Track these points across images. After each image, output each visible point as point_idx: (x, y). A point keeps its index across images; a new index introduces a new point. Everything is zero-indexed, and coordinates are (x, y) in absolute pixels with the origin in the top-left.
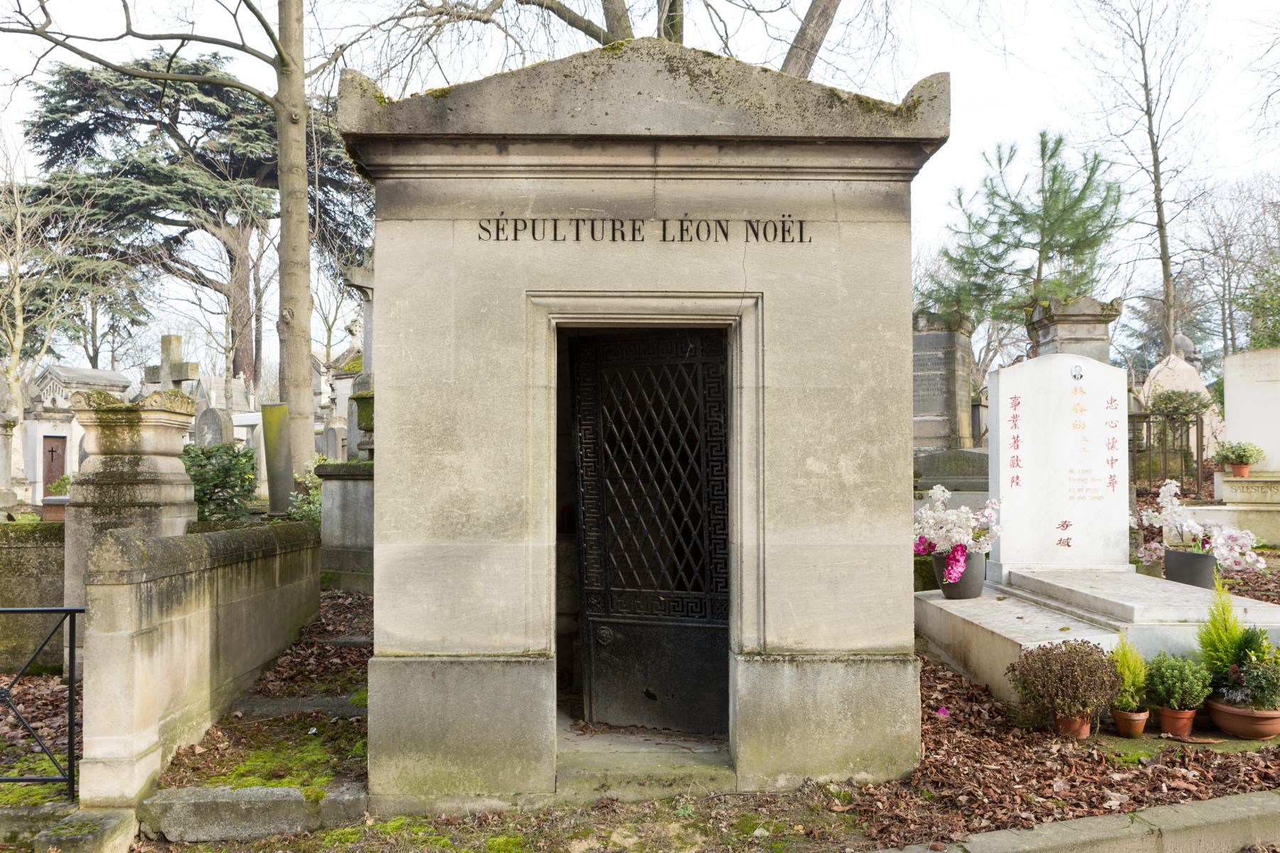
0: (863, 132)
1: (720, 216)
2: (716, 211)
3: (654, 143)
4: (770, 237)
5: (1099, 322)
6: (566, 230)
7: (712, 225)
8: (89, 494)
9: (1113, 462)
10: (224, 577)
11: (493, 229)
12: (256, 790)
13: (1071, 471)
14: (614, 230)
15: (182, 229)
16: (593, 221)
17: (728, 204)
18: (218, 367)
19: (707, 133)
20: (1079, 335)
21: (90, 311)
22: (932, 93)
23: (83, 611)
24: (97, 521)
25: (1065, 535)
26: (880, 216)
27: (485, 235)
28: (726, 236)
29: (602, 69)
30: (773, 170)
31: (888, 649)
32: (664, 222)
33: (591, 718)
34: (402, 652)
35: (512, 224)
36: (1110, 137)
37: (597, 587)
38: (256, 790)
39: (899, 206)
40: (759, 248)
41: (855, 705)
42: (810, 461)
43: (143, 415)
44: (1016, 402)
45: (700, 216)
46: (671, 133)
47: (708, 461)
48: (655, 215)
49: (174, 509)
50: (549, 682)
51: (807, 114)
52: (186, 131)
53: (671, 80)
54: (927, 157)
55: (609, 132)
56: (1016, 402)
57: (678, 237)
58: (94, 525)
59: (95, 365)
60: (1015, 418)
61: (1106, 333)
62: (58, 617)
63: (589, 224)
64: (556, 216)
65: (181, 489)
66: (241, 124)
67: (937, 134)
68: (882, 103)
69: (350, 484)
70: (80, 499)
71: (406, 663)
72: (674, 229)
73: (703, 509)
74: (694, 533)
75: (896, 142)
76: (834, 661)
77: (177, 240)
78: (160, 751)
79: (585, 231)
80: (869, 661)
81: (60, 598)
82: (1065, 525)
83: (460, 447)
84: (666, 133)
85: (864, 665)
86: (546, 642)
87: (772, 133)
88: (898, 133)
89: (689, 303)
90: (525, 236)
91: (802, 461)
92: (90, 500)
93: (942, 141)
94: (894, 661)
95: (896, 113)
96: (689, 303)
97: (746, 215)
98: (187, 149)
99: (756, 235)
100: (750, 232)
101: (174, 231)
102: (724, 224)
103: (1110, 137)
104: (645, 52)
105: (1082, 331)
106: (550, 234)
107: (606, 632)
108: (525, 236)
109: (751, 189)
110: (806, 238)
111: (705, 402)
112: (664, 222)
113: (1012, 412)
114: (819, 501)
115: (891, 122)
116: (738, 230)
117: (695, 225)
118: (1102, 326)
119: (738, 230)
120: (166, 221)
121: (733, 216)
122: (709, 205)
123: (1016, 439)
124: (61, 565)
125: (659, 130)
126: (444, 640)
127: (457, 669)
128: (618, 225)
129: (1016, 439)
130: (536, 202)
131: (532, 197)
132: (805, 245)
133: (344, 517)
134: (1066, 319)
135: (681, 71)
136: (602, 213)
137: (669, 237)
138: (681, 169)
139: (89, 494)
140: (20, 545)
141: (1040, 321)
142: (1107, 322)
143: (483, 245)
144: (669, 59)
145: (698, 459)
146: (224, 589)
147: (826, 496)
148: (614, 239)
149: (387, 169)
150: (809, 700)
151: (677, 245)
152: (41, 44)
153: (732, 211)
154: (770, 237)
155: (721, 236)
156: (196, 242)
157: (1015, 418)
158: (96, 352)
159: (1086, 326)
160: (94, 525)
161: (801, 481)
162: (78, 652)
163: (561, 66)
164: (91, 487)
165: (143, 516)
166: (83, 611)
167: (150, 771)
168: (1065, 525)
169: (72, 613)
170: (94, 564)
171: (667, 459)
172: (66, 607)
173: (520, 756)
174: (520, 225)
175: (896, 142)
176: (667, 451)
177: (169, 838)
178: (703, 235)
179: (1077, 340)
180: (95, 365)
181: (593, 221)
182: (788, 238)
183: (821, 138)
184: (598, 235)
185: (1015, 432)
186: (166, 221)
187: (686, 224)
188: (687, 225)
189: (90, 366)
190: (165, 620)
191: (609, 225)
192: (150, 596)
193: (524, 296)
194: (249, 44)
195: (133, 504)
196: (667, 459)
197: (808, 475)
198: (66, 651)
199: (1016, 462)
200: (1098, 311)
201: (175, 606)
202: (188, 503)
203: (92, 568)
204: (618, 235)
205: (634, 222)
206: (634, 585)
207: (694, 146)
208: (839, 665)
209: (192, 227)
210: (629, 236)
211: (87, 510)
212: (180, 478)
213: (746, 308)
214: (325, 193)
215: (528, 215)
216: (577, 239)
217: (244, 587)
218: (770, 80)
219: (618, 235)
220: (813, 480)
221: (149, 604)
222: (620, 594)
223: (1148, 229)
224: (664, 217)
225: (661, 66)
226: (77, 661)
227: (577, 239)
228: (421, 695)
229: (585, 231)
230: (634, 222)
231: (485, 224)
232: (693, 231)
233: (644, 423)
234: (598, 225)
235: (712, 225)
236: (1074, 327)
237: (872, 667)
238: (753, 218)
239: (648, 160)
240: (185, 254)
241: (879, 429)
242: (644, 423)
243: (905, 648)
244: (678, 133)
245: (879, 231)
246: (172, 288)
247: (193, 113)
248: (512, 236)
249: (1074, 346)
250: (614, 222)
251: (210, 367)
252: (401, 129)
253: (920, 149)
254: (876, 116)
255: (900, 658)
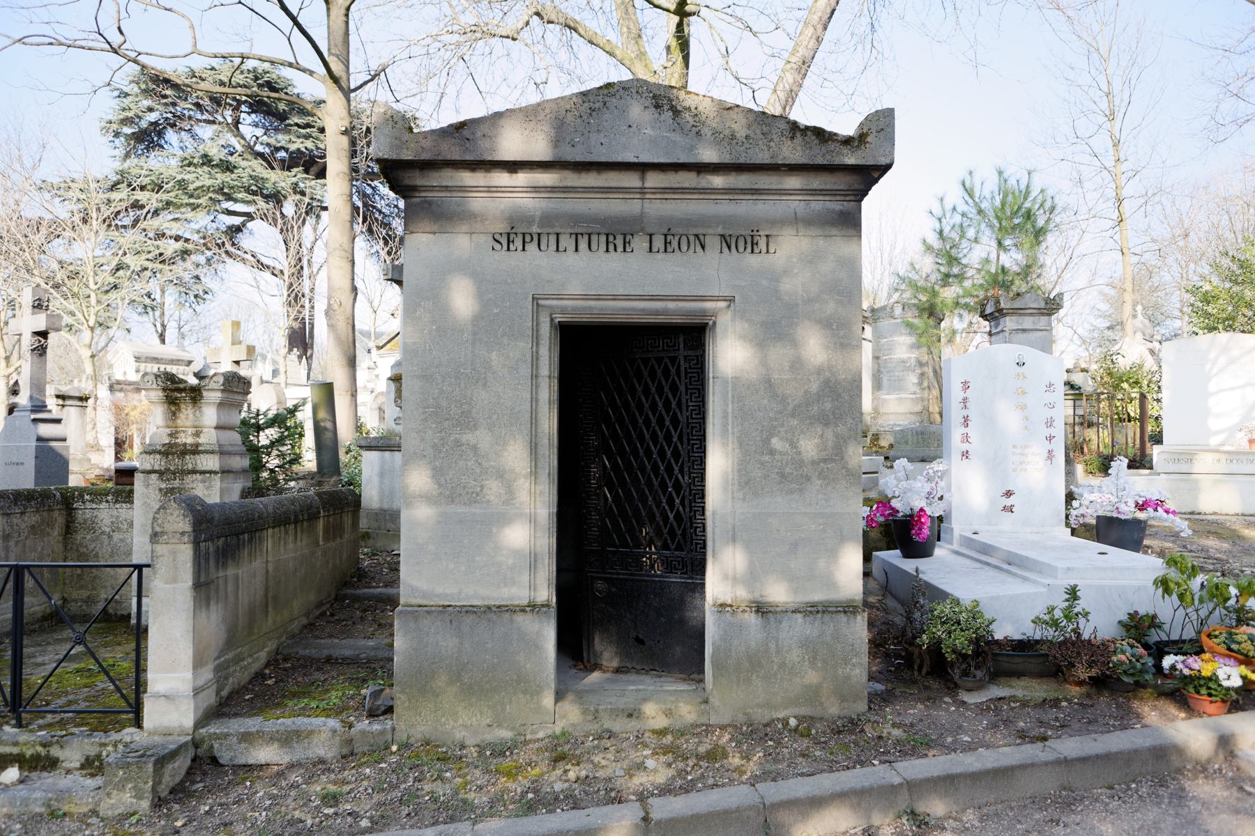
0: (820, 160)
1: (700, 231)
2: (696, 226)
3: (643, 168)
4: (741, 249)
5: (1043, 314)
6: (567, 242)
7: (692, 238)
8: (156, 462)
9: (1050, 438)
10: (273, 537)
11: (505, 242)
12: (1007, 754)
13: (1014, 447)
14: (607, 243)
15: (241, 219)
16: (590, 235)
17: (704, 221)
18: (275, 342)
19: (687, 161)
20: (1025, 326)
21: (159, 292)
22: (881, 124)
23: (148, 566)
24: (163, 486)
25: (1008, 502)
26: (834, 231)
27: (497, 246)
28: (703, 247)
29: (597, 105)
30: (743, 191)
31: (840, 602)
32: (651, 235)
33: (589, 661)
34: (424, 602)
35: (520, 237)
36: (1075, 140)
37: (595, 547)
38: (1007, 754)
39: (850, 222)
40: (731, 257)
41: (812, 649)
42: (774, 441)
43: (205, 394)
44: (966, 386)
45: (681, 231)
46: (656, 161)
47: (689, 440)
48: (642, 230)
49: (231, 476)
50: (547, 634)
51: (772, 144)
52: (246, 130)
53: (657, 115)
54: (876, 181)
55: (603, 159)
56: (966, 386)
57: (662, 249)
58: (160, 490)
59: (163, 341)
60: (965, 400)
61: (1050, 324)
62: (128, 570)
63: (586, 237)
64: (558, 230)
65: (238, 458)
66: (297, 125)
67: (883, 161)
68: (836, 134)
69: (387, 454)
70: (149, 467)
71: (428, 612)
72: (658, 242)
73: (685, 480)
74: (677, 501)
75: (846, 170)
76: (793, 612)
77: (238, 229)
78: (215, 687)
79: (583, 245)
80: (824, 612)
81: (129, 553)
82: (1009, 494)
83: (475, 427)
84: (651, 161)
85: (819, 615)
86: (545, 593)
87: (742, 161)
88: (851, 160)
89: (671, 305)
90: (532, 247)
91: (767, 441)
92: (157, 468)
93: (888, 167)
94: (845, 612)
95: (847, 141)
96: (671, 305)
97: (720, 230)
98: (250, 148)
99: (729, 248)
100: (724, 245)
101: (237, 221)
102: (702, 238)
103: (1075, 140)
104: (634, 91)
105: (1028, 322)
106: (553, 246)
107: (600, 585)
108: (532, 247)
109: (725, 208)
110: (772, 250)
111: (687, 389)
112: (651, 235)
113: (962, 395)
114: (783, 475)
115: (845, 150)
116: (713, 242)
117: (677, 238)
118: (1046, 318)
119: (713, 242)
120: (230, 213)
121: (710, 231)
122: (689, 222)
123: (966, 419)
124: (131, 525)
125: (646, 158)
126: (460, 593)
127: (471, 617)
128: (611, 238)
129: (966, 419)
130: (542, 218)
131: (538, 214)
132: (771, 256)
133: (381, 483)
134: (1016, 312)
135: (666, 107)
136: (597, 228)
137: (655, 249)
138: (665, 190)
139: (156, 462)
140: (94, 506)
141: (991, 314)
142: (1050, 315)
143: (496, 255)
144: (654, 97)
145: (680, 438)
146: (273, 547)
147: (788, 470)
148: (607, 250)
149: (415, 188)
150: (772, 646)
151: (661, 256)
152: (116, 60)
153: (709, 227)
154: (741, 249)
155: (699, 248)
156: (255, 230)
157: (965, 400)
158: (164, 326)
159: (1031, 319)
160: (160, 490)
161: (767, 458)
162: (144, 600)
163: (562, 103)
164: (158, 457)
165: (203, 481)
166: (148, 566)
167: (205, 705)
168: (1009, 494)
169: (139, 568)
170: (159, 526)
171: (654, 437)
172: (135, 562)
173: (525, 692)
174: (528, 238)
175: (846, 170)
176: (654, 431)
177: (221, 761)
178: (684, 248)
179: (1024, 330)
180: (163, 341)
181: (590, 235)
182: (756, 250)
183: (784, 165)
184: (594, 246)
185: (965, 413)
186: (230, 213)
187: (669, 238)
188: (672, 237)
189: (158, 341)
190: (221, 574)
191: (603, 238)
192: (207, 553)
193: (530, 299)
194: (303, 64)
195: (194, 472)
196: (654, 437)
197: (772, 452)
198: (135, 600)
199: (966, 439)
200: (1042, 305)
201: (230, 562)
202: (244, 471)
203: (158, 529)
204: (611, 247)
205: (625, 235)
206: (627, 546)
207: (676, 171)
208: (799, 616)
209: (250, 216)
210: (620, 248)
211: (154, 476)
212: (237, 448)
213: (721, 309)
214: (373, 188)
215: (535, 229)
216: (577, 250)
217: (291, 545)
218: (741, 115)
219: (611, 247)
220: (777, 457)
221: (207, 560)
222: (614, 553)
223: (1111, 223)
224: (651, 231)
225: (648, 102)
226: (144, 608)
227: (577, 250)
228: (446, 642)
229: (583, 245)
230: (625, 235)
231: (497, 237)
232: (675, 243)
233: (626, 408)
234: (594, 238)
235: (692, 238)
236: (1021, 319)
237: (827, 617)
238: (727, 232)
239: (638, 184)
240: (245, 240)
241: (834, 413)
242: (626, 408)
243: (854, 601)
244: (662, 160)
245: (839, 246)
246: (235, 272)
247: (253, 116)
248: (520, 247)
249: (1021, 336)
250: (607, 235)
251: (267, 343)
252: (425, 156)
253: (871, 174)
254: (832, 146)
255: (848, 609)
